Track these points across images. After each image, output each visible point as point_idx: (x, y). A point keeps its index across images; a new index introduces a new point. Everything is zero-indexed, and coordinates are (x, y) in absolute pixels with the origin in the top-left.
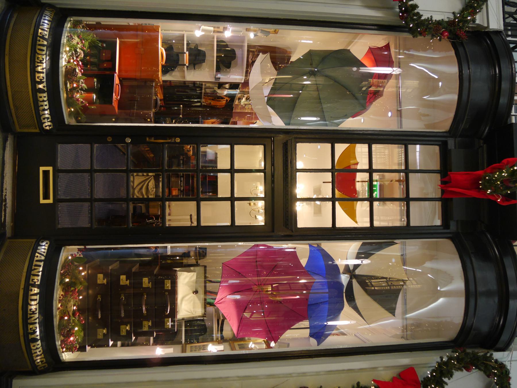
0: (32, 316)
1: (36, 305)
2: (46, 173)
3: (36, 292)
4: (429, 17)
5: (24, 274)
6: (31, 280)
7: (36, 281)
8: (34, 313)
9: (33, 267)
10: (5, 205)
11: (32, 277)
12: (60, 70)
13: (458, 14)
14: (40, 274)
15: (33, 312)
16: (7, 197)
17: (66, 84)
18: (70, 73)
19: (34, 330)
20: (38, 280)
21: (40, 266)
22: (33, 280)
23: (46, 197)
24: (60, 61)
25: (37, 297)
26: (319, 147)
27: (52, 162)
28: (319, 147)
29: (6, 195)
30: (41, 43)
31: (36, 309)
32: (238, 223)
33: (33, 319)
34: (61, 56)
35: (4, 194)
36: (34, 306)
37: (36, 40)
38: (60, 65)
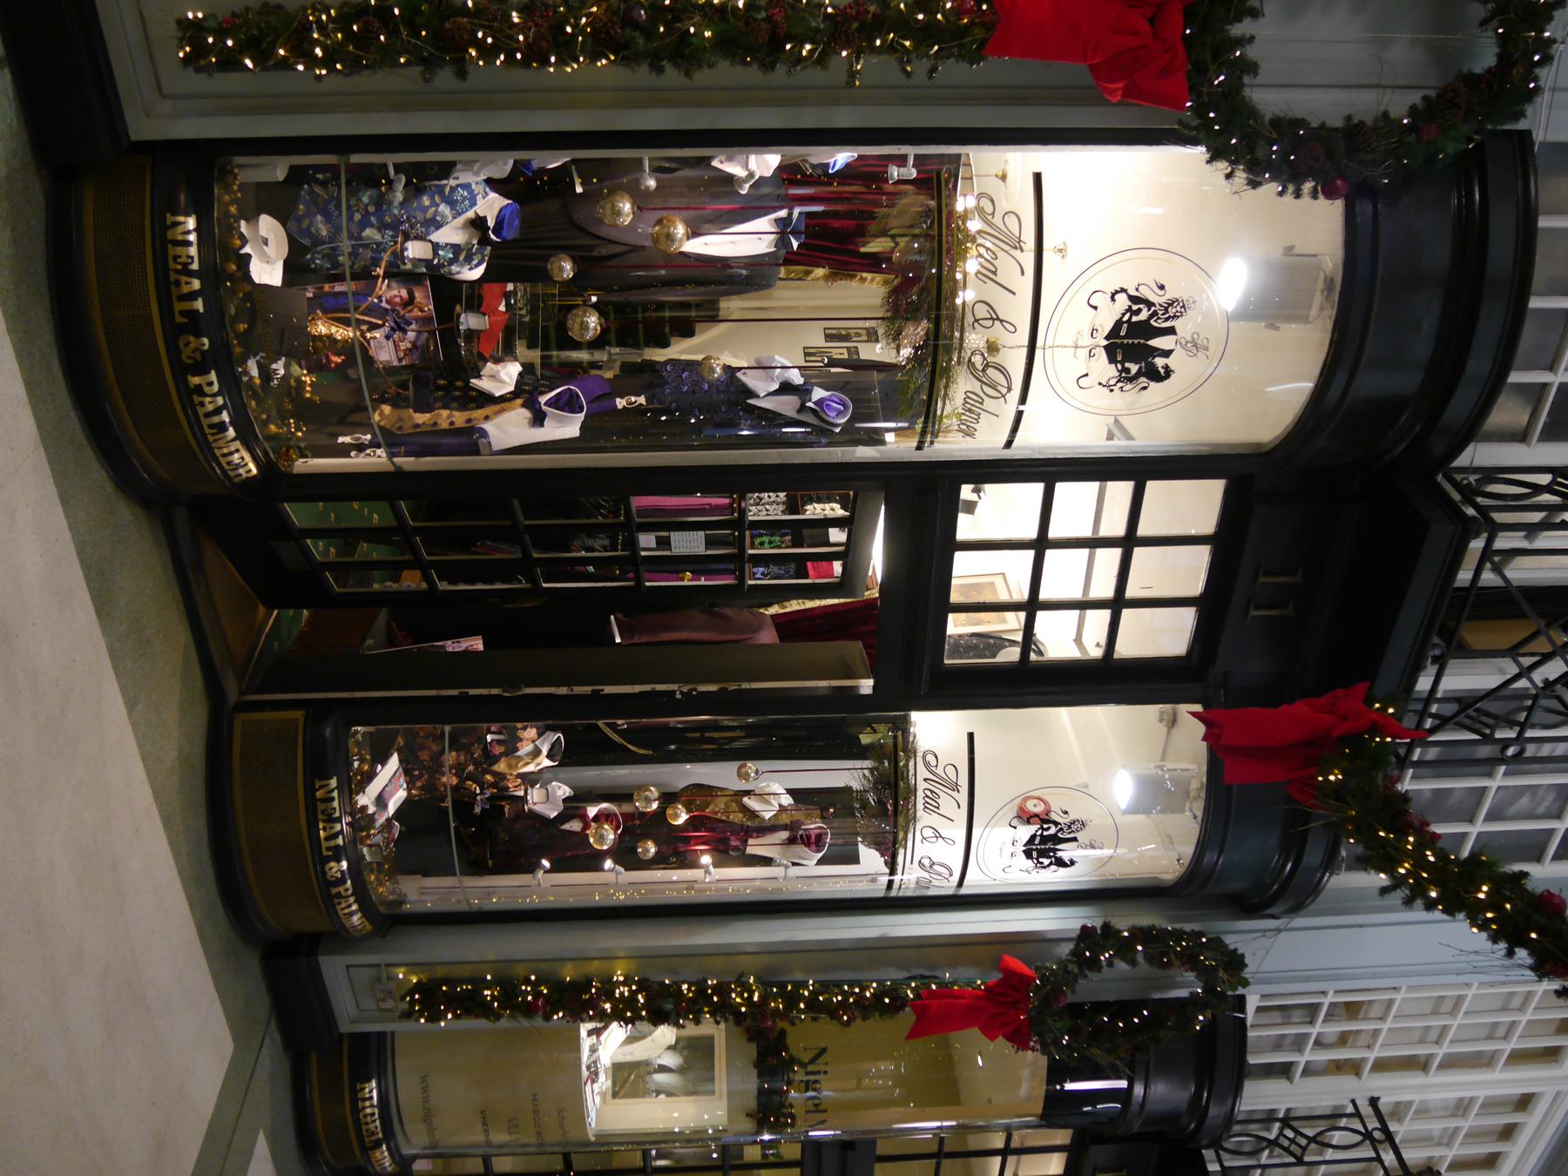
7: (183, 260)
11: (172, 251)
14: (192, 237)
32: (959, 557)
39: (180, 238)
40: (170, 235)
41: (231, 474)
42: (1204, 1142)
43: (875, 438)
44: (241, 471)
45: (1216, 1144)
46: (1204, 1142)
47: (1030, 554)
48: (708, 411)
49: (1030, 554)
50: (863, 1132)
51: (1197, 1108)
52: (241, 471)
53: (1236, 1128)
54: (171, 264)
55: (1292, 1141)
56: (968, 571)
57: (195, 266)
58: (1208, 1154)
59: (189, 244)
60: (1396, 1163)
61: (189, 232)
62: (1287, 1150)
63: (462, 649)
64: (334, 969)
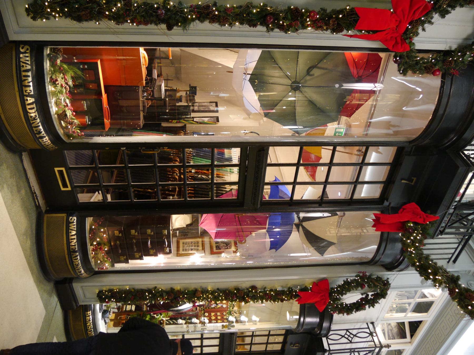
0: (34, 121)
1: (35, 112)
2: (61, 172)
3: (31, 101)
4: (433, 21)
5: (65, 245)
6: (24, 92)
7: (29, 91)
8: (35, 119)
9: (70, 241)
10: (36, 196)
11: (24, 89)
12: (53, 117)
13: (430, 279)
14: (31, 84)
15: (34, 118)
16: (36, 191)
17: (60, 123)
18: (62, 116)
19: (39, 131)
20: (31, 91)
21: (29, 76)
22: (26, 91)
23: (65, 185)
24: (51, 110)
25: (75, 237)
26: (339, 194)
27: (64, 164)
28: (339, 194)
29: (34, 190)
30: (25, 68)
31: (36, 116)
32: (268, 169)
33: (36, 123)
34: (50, 105)
35: (33, 189)
36: (33, 113)
37: (20, 66)
38: (52, 113)
39: (27, 84)
40: (23, 83)
41: (43, 144)
42: (323, 335)
43: (190, 163)
44: (46, 143)
45: (327, 336)
46: (323, 335)
47: (295, 168)
48: (316, 20)
49: (295, 168)
50: (32, 231)
51: (320, 325)
52: (46, 143)
53: (331, 333)
54: (30, 119)
55: (349, 336)
56: (270, 175)
57: (32, 93)
58: (324, 339)
59: (30, 86)
60: (379, 343)
61: (29, 82)
62: (347, 339)
63: (121, 188)
64: (77, 287)
